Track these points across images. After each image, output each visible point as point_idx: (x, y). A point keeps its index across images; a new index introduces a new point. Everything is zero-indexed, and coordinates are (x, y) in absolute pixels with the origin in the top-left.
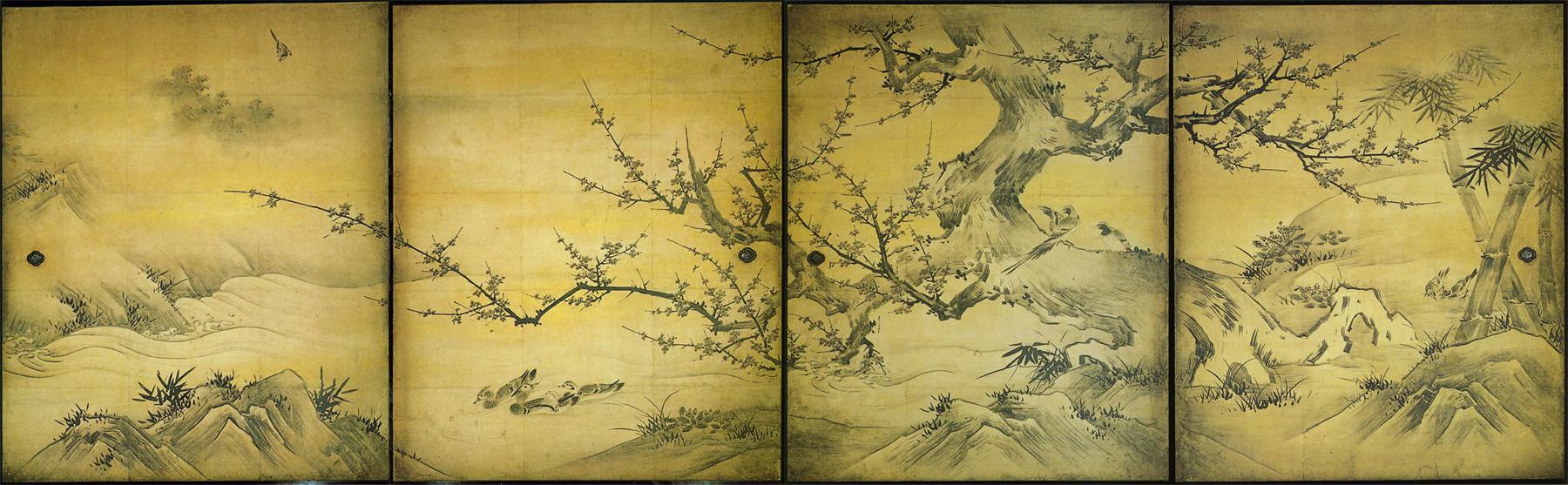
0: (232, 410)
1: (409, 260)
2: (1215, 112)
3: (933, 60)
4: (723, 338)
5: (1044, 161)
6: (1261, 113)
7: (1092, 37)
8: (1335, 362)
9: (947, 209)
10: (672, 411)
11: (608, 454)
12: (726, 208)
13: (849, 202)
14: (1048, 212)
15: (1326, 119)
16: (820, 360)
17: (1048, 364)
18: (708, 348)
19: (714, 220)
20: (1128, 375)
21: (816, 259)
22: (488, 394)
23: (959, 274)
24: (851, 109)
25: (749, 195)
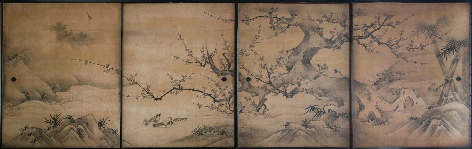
0: (73, 126)
1: (125, 81)
2: (365, 35)
3: (284, 20)
4: (217, 104)
5: (317, 50)
6: (379, 36)
7: (332, 13)
8: (401, 111)
9: (289, 65)
10: (201, 126)
11: (182, 140)
12: (218, 66)
13: (259, 63)
14: (319, 66)
15: (398, 39)
16: (250, 110)
17: (319, 112)
18: (212, 107)
19: (214, 69)
20: (343, 115)
21: (249, 79)
22: (146, 121)
23: (292, 84)
24: (259, 35)
25: (225, 61)
